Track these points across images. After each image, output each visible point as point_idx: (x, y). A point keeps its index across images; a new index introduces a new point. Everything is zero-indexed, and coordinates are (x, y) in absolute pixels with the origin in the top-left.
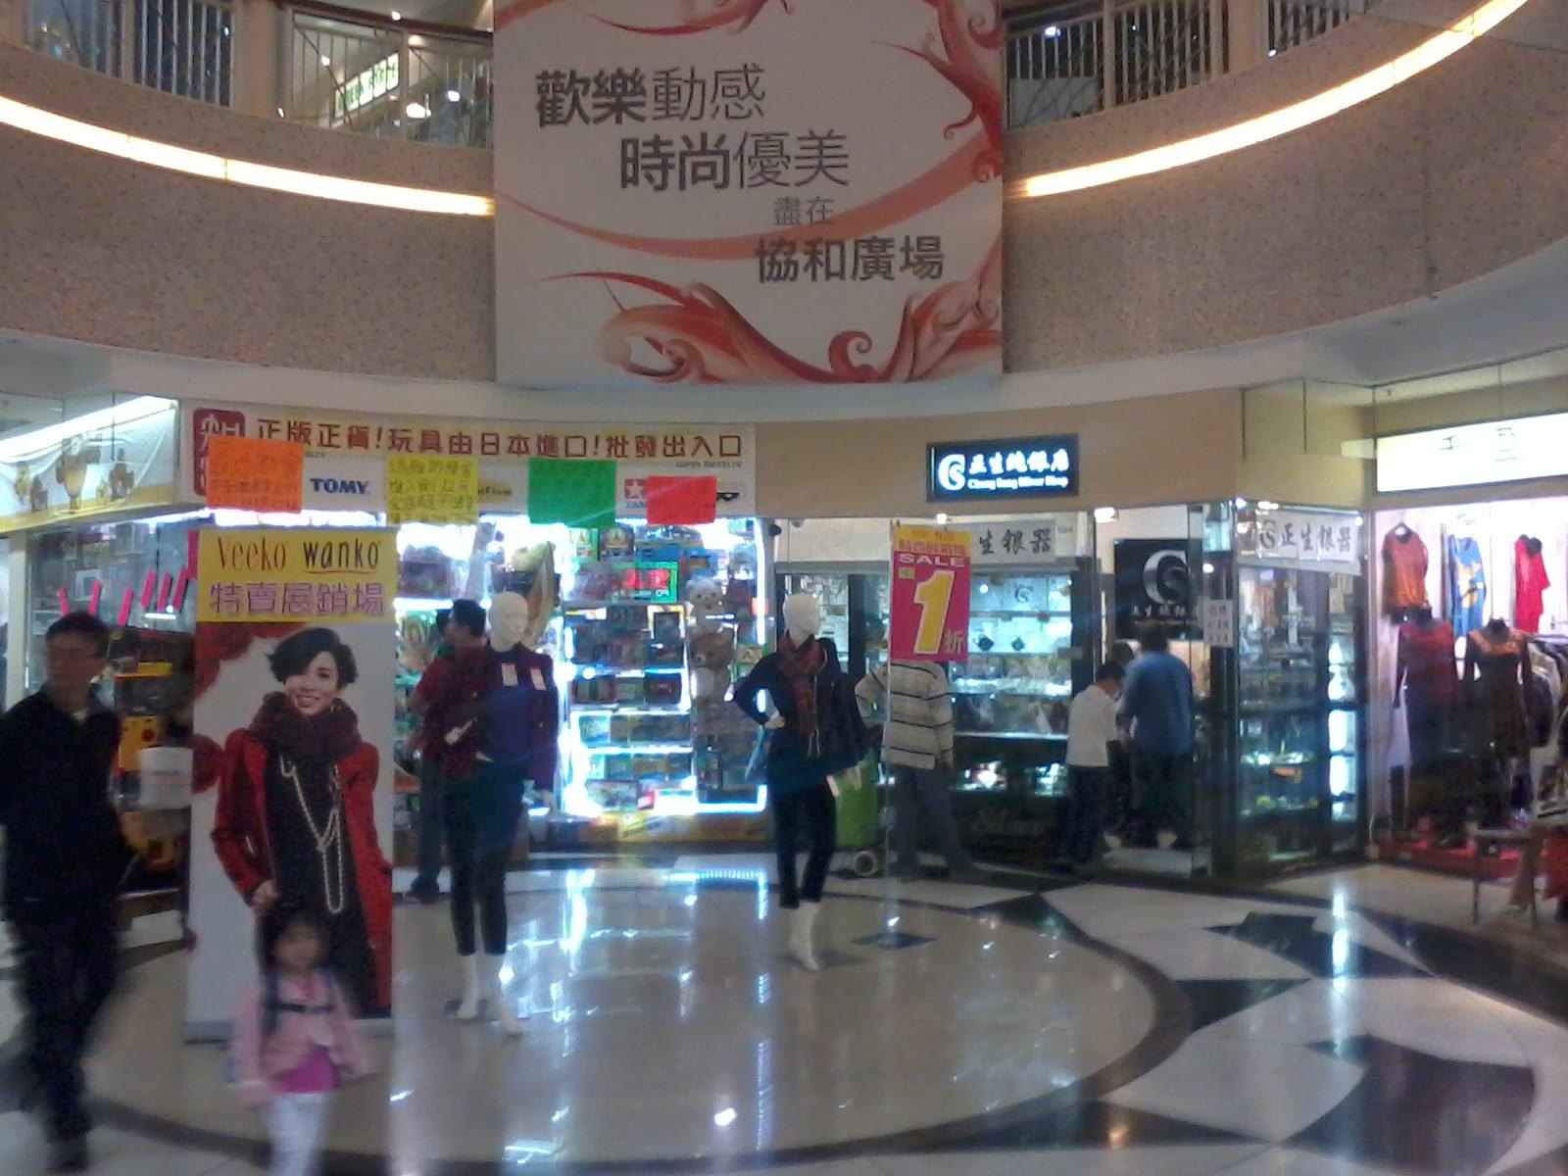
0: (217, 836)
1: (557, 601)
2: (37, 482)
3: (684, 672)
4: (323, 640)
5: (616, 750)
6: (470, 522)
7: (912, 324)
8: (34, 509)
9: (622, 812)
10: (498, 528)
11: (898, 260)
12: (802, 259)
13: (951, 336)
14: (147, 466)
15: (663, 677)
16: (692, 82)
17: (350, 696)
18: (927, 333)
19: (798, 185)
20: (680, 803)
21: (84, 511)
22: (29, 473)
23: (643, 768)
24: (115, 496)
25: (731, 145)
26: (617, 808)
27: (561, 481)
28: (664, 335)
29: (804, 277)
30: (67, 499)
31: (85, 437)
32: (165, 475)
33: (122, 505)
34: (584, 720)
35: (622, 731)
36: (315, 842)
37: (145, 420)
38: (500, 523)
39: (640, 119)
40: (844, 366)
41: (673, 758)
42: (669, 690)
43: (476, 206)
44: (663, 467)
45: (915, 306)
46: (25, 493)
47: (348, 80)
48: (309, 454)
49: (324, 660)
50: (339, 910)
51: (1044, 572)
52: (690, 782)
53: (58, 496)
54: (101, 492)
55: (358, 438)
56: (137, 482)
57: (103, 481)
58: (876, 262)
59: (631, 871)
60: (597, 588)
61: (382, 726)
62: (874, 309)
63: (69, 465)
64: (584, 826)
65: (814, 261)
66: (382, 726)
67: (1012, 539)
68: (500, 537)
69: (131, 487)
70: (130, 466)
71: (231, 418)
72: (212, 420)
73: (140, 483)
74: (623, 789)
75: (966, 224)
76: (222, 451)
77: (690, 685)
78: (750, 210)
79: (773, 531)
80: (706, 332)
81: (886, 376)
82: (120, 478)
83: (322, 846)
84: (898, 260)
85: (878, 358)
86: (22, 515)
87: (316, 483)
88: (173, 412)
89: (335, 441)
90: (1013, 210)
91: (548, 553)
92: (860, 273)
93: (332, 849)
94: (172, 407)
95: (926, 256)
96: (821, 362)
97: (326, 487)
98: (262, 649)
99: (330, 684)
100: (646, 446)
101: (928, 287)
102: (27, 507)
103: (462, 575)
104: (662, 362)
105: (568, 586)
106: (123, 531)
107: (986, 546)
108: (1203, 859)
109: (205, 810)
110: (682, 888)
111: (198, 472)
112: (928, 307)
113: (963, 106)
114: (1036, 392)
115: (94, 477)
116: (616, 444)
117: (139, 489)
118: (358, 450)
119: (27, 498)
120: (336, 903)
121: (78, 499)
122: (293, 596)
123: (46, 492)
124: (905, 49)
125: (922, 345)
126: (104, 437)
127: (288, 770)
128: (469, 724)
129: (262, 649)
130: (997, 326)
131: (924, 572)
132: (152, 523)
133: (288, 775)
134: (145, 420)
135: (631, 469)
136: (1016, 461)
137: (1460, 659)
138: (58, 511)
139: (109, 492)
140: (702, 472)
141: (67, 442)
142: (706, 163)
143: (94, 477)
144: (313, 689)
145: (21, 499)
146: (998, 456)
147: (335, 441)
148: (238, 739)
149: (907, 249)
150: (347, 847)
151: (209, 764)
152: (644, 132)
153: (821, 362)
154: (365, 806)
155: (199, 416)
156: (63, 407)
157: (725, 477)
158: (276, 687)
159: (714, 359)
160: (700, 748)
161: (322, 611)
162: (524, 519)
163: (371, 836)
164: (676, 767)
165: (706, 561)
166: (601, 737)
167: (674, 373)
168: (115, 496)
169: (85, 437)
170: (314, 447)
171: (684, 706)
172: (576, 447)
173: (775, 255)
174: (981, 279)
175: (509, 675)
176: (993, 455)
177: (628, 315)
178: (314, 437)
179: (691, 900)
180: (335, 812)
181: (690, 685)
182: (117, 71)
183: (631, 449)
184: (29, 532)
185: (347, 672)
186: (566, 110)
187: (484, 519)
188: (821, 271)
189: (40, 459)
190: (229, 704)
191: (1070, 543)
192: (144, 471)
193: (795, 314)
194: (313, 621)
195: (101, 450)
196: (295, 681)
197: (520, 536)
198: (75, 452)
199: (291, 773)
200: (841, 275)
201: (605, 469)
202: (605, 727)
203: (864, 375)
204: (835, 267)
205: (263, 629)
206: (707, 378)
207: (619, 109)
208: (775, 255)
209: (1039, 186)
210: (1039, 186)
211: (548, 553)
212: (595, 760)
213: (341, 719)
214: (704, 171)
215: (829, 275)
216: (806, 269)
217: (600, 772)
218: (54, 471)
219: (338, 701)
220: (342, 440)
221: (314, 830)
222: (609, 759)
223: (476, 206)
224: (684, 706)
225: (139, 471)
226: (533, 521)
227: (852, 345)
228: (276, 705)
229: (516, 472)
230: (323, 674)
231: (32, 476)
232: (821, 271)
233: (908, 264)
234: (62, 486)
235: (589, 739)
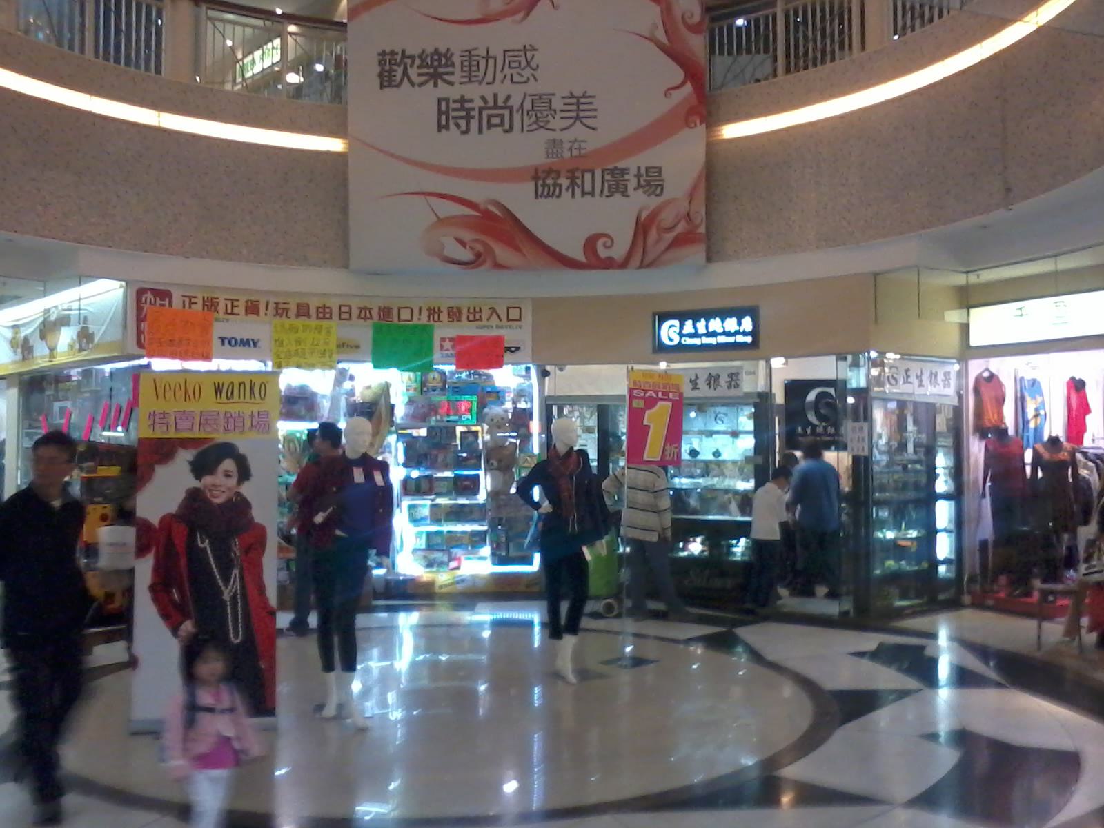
0: (153, 588)
1: (392, 423)
2: (26, 339)
3: (481, 473)
4: (228, 450)
5: (434, 528)
6: (331, 367)
7: (642, 228)
8: (24, 359)
9: (438, 572)
10: (351, 372)
11: (633, 183)
12: (565, 182)
13: (669, 237)
14: (104, 328)
15: (467, 477)
16: (487, 58)
17: (246, 490)
18: (653, 234)
19: (562, 130)
20: (479, 565)
21: (59, 360)
22: (20, 333)
23: (453, 541)
24: (81, 350)
25: (515, 102)
26: (434, 569)
28: (467, 236)
29: (566, 195)
30: (47, 352)
31: (60, 308)
32: (116, 334)
33: (86, 356)
34: (411, 507)
35: (438, 515)
36: (221, 593)
37: (102, 296)
38: (352, 368)
39: (451, 83)
40: (594, 258)
41: (474, 534)
42: (471, 486)
43: (335, 145)
44: (467, 329)
45: (644, 215)
46: (18, 347)
47: (245, 56)
48: (217, 320)
49: (228, 464)
50: (238, 641)
51: (735, 403)
52: (486, 551)
53: (41, 350)
54: (71, 347)
55: (252, 309)
56: (96, 340)
57: (72, 339)
58: (616, 185)
59: (444, 613)
60: (420, 414)
61: (269, 511)
62: (615, 218)
63: (48, 328)
64: (411, 582)
65: (573, 184)
66: (269, 511)
67: (713, 379)
68: (352, 378)
69: (92, 343)
70: (92, 328)
71: (163, 294)
72: (149, 296)
73: (99, 340)
74: (438, 556)
75: (680, 158)
76: (156, 318)
77: (486, 483)
78: (528, 148)
79: (544, 374)
80: (497, 234)
81: (624, 264)
82: (85, 336)
83: (227, 596)
84: (633, 183)
85: (618, 252)
86: (15, 362)
87: (223, 340)
88: (122, 290)
89: (236, 310)
90: (713, 148)
91: (386, 389)
92: (606, 192)
93: (234, 598)
94: (121, 286)
95: (652, 180)
96: (578, 255)
97: (230, 343)
98: (185, 457)
99: (233, 482)
100: (455, 314)
101: (654, 202)
102: (19, 357)
103: (326, 405)
104: (466, 255)
105: (400, 412)
106: (87, 374)
107: (694, 384)
108: (847, 605)
109: (144, 570)
110: (480, 625)
111: (139, 332)
112: (653, 216)
113: (678, 74)
114: (729, 276)
115: (66, 336)
116: (434, 313)
117: (98, 344)
118: (252, 317)
119: (19, 350)
120: (236, 636)
121: (55, 352)
122: (206, 419)
123: (33, 346)
125: (649, 243)
126: (73, 308)
127: (203, 542)
128: (330, 510)
129: (185, 457)
130: (702, 230)
131: (651, 403)
132: (107, 368)
133: (203, 546)
134: (102, 296)
135: (444, 330)
136: (715, 324)
137: (1028, 464)
138: (41, 360)
139: (77, 346)
140: (495, 333)
141: (47, 311)
142: (497, 115)
143: (66, 336)
144: (220, 485)
145: (15, 352)
146: (703, 321)
147: (236, 310)
148: (167, 521)
149: (638, 176)
150: (244, 596)
151: (147, 538)
152: (453, 93)
153: (578, 255)
154: (257, 568)
155: (140, 293)
156: (45, 287)
157: (510, 336)
158: (195, 483)
159: (502, 253)
160: (493, 526)
161: (227, 430)
162: (369, 366)
163: (261, 588)
164: (476, 540)
165: (497, 395)
166: (423, 519)
167: (475, 263)
168: (81, 350)
169: (60, 308)
170: (221, 315)
171: (482, 497)
172: (405, 315)
173: (545, 179)
174: (691, 197)
175: (358, 476)
176: (699, 321)
177: (442, 222)
178: (221, 308)
179: (486, 634)
180: (236, 572)
181: (486, 483)
182: (82, 50)
183: (444, 316)
184: (20, 374)
185: (244, 473)
186: (398, 77)
187: (341, 366)
188: (578, 191)
189: (28, 323)
190: (161, 496)
191: (753, 383)
192: (101, 332)
193: (560, 221)
194: (220, 437)
195: (71, 317)
196: (208, 480)
197: (366, 377)
198: (53, 318)
199: (205, 544)
200: (592, 193)
201: (426, 330)
202: (426, 512)
203: (608, 264)
204: (588, 188)
205: (185, 443)
206: (498, 266)
207: (436, 77)
208: (545, 179)
209: (732, 131)
210: (732, 131)
211: (386, 389)
212: (419, 535)
213: (240, 506)
214: (496, 121)
215: (584, 193)
216: (567, 189)
217: (422, 543)
218: (38, 331)
219: (238, 494)
220: (241, 310)
221: (221, 584)
222: (429, 535)
223: (335, 145)
224: (482, 497)
225: (98, 332)
226: (375, 367)
227: (600, 243)
228: (194, 496)
229: (363, 332)
230: (227, 475)
231: (23, 335)
232: (578, 191)
233: (639, 186)
234: (44, 342)
235: (415, 520)
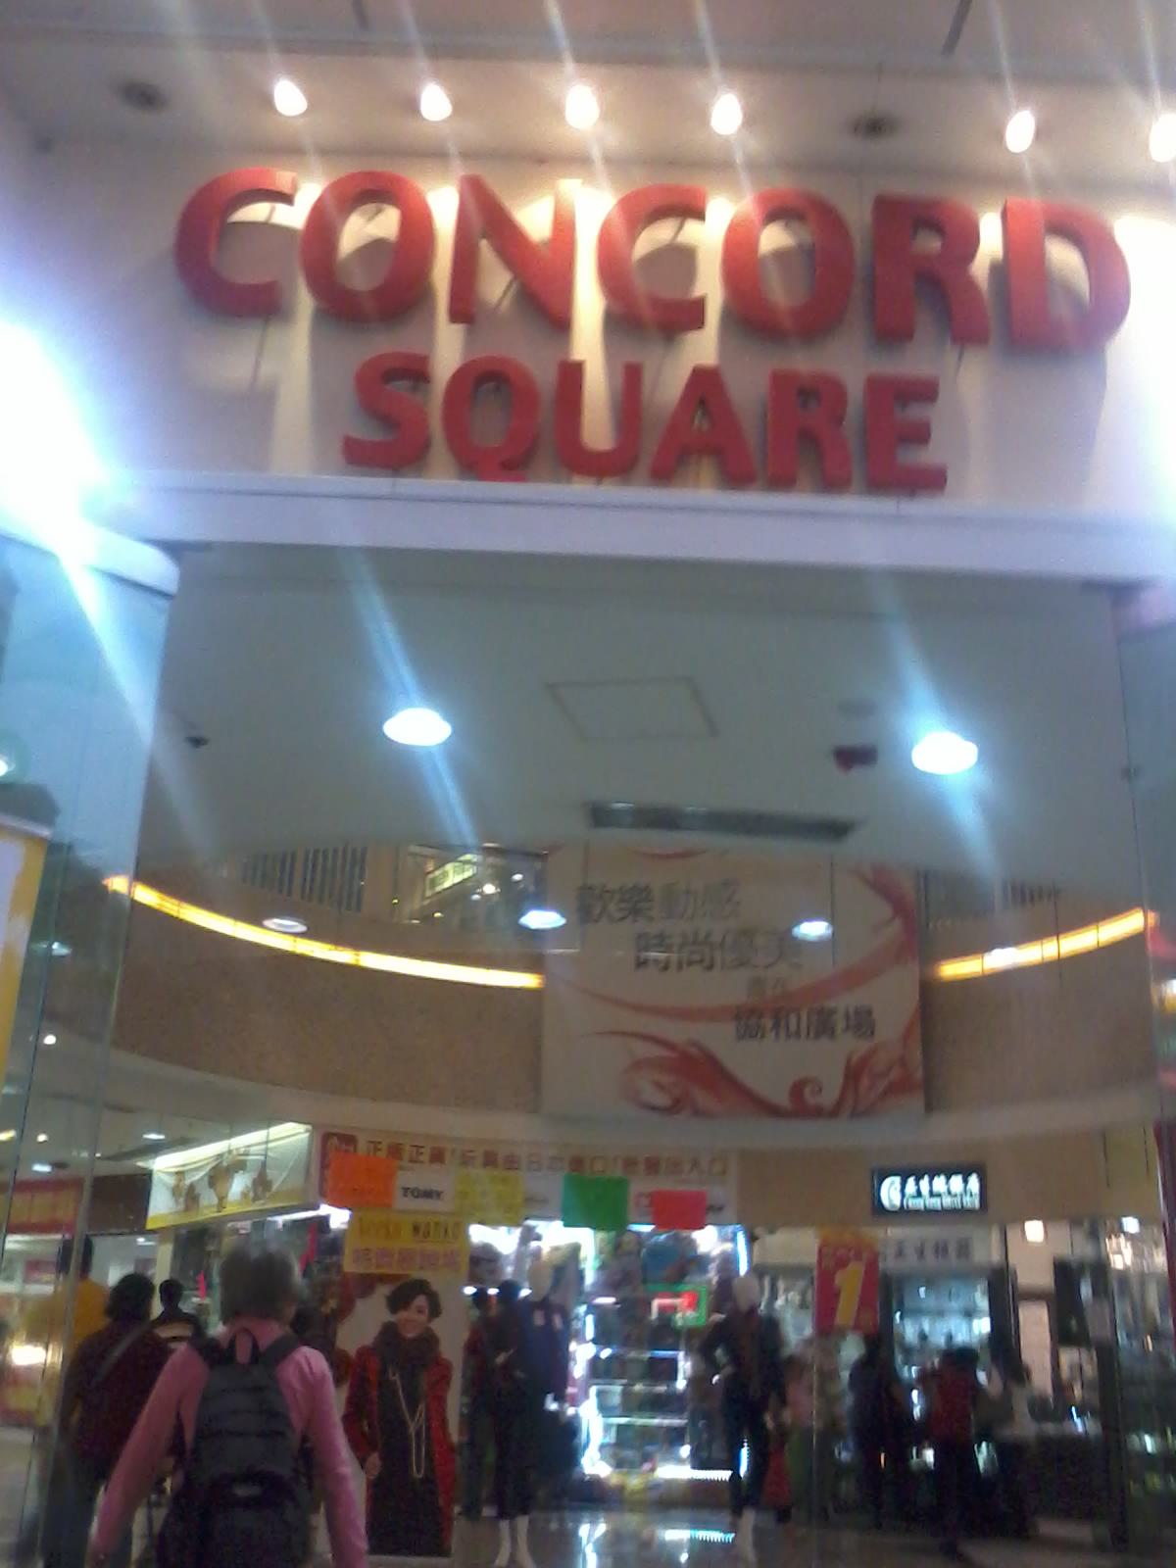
0: (346, 1418)
1: (580, 1292)
2: (192, 1187)
3: (681, 1355)
4: (421, 1287)
5: (623, 1420)
6: (518, 1225)
7: (853, 1074)
8: (187, 1209)
9: (628, 1473)
10: (538, 1230)
11: (840, 1025)
12: (768, 1023)
13: (882, 1085)
14: (284, 1175)
15: (664, 1360)
16: (688, 892)
17: (437, 1326)
18: (865, 1082)
19: (767, 967)
20: (677, 1470)
21: (229, 1210)
22: (185, 1179)
23: (647, 1435)
24: (256, 1198)
25: (716, 938)
26: (625, 1470)
27: (590, 1203)
28: (666, 1079)
29: (772, 1035)
30: (215, 1201)
31: (235, 1152)
32: (298, 1181)
33: (263, 1204)
34: (599, 1394)
35: (631, 1404)
36: (403, 1424)
37: (289, 1136)
38: (540, 1226)
39: (651, 919)
40: (800, 1106)
41: (670, 1429)
42: (670, 1370)
43: (528, 980)
44: (666, 1184)
45: (855, 1059)
46: (180, 1195)
47: (436, 869)
48: (401, 1168)
49: (421, 1301)
50: (420, 1476)
51: (966, 1276)
52: (685, 1451)
53: (208, 1199)
54: (244, 1195)
55: (437, 1157)
56: (275, 1187)
57: (247, 1187)
58: (823, 1026)
59: (632, 1520)
60: (612, 1281)
61: (452, 1338)
62: (825, 1062)
63: (220, 1173)
64: (595, 1483)
65: (776, 1026)
66: (452, 1338)
67: (941, 1250)
68: (538, 1238)
69: (269, 1191)
70: (270, 1173)
71: (349, 1140)
72: (335, 1140)
73: (280, 1186)
74: (629, 1454)
75: (892, 1001)
76: (338, 1164)
77: (685, 1366)
78: (729, 988)
79: (752, 1239)
80: (697, 1080)
81: (834, 1113)
82: (261, 1183)
83: (412, 1430)
84: (840, 1025)
85: (829, 1096)
86: (177, 1212)
87: (406, 1190)
88: (307, 1135)
89: (422, 1158)
90: (931, 992)
91: (575, 1250)
92: (812, 1035)
93: (418, 1434)
94: (307, 1131)
95: (862, 1022)
96: (782, 1099)
97: (412, 1192)
98: (383, 1291)
99: (423, 1318)
100: (653, 1166)
101: (862, 1046)
102: (181, 1207)
103: (509, 1271)
104: (662, 1100)
105: (590, 1278)
106: (260, 1226)
107: (921, 1253)
108: (1104, 1530)
109: (336, 1400)
110: (678, 1546)
111: (323, 1179)
112: (865, 1061)
113: (885, 910)
114: (946, 1130)
115: (239, 1184)
116: (630, 1164)
117: (277, 1192)
118: (436, 1166)
119: (182, 1200)
120: (418, 1471)
121: (225, 1200)
122: (406, 1257)
123: (199, 1195)
124: (614, 1033)
125: (863, 1090)
126: (251, 1152)
127: (394, 1374)
128: (512, 1351)
129: (383, 1291)
130: (919, 1074)
131: (842, 1263)
132: (281, 1220)
133: (394, 1378)
134: (289, 1136)
135: (640, 1186)
136: (939, 1183)
138: (207, 1209)
139: (251, 1195)
140: (693, 1188)
141: (220, 1156)
142: (701, 954)
143: (239, 1184)
144: (412, 1320)
145: (177, 1201)
146: (942, 1178)
147: (422, 1158)
148: (364, 1352)
149: (847, 1016)
150: (428, 1428)
151: (340, 1365)
152: (653, 929)
153: (782, 1099)
154: (441, 1400)
155: (326, 1137)
156: (231, 1128)
157: (716, 1193)
158: (392, 1318)
159: (702, 1098)
160: (693, 1420)
161: (421, 1268)
162: (559, 1224)
163: (444, 1422)
164: (675, 1437)
165: (700, 1262)
166: (614, 1408)
167: (674, 1108)
168: (256, 1198)
169: (235, 1152)
170: (405, 1163)
171: (681, 1384)
172: (599, 1166)
173: (749, 1019)
174: (906, 1037)
175: (538, 1319)
176: (922, 1177)
177: (638, 1065)
178: (406, 1156)
179: (684, 1557)
180: (421, 1407)
181: (685, 1366)
182: (290, 893)
183: (642, 1167)
184: (176, 1228)
185: (435, 1310)
186: (597, 911)
187: (531, 1223)
188: (782, 1034)
189: (197, 1169)
190: (363, 1326)
191: (987, 1250)
192: (281, 1179)
193: (765, 1064)
194: (416, 1274)
195: (248, 1164)
196: (403, 1315)
197: (554, 1235)
198: (225, 1164)
199: (396, 1378)
200: (798, 1034)
201: (621, 1184)
202: (616, 1400)
203: (818, 1113)
204: (793, 1027)
205: (382, 1279)
206: (697, 1113)
207: (635, 912)
208: (749, 1019)
209: (954, 969)
210: (954, 969)
211: (575, 1250)
212: (607, 1428)
213: (429, 1341)
214: (696, 957)
215: (788, 1036)
216: (771, 1031)
217: (612, 1438)
218: (206, 1179)
219: (429, 1330)
220: (425, 1158)
221: (408, 1417)
222: (620, 1427)
223: (528, 980)
224: (681, 1384)
225: (277, 1179)
226: (566, 1225)
227: (807, 1091)
228: (389, 1333)
229: (553, 1184)
230: (420, 1311)
231: (188, 1182)
232: (782, 1034)
233: (847, 1028)
234: (212, 1191)
235: (604, 1409)
